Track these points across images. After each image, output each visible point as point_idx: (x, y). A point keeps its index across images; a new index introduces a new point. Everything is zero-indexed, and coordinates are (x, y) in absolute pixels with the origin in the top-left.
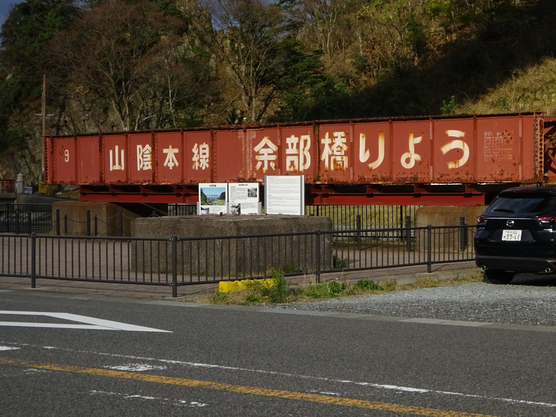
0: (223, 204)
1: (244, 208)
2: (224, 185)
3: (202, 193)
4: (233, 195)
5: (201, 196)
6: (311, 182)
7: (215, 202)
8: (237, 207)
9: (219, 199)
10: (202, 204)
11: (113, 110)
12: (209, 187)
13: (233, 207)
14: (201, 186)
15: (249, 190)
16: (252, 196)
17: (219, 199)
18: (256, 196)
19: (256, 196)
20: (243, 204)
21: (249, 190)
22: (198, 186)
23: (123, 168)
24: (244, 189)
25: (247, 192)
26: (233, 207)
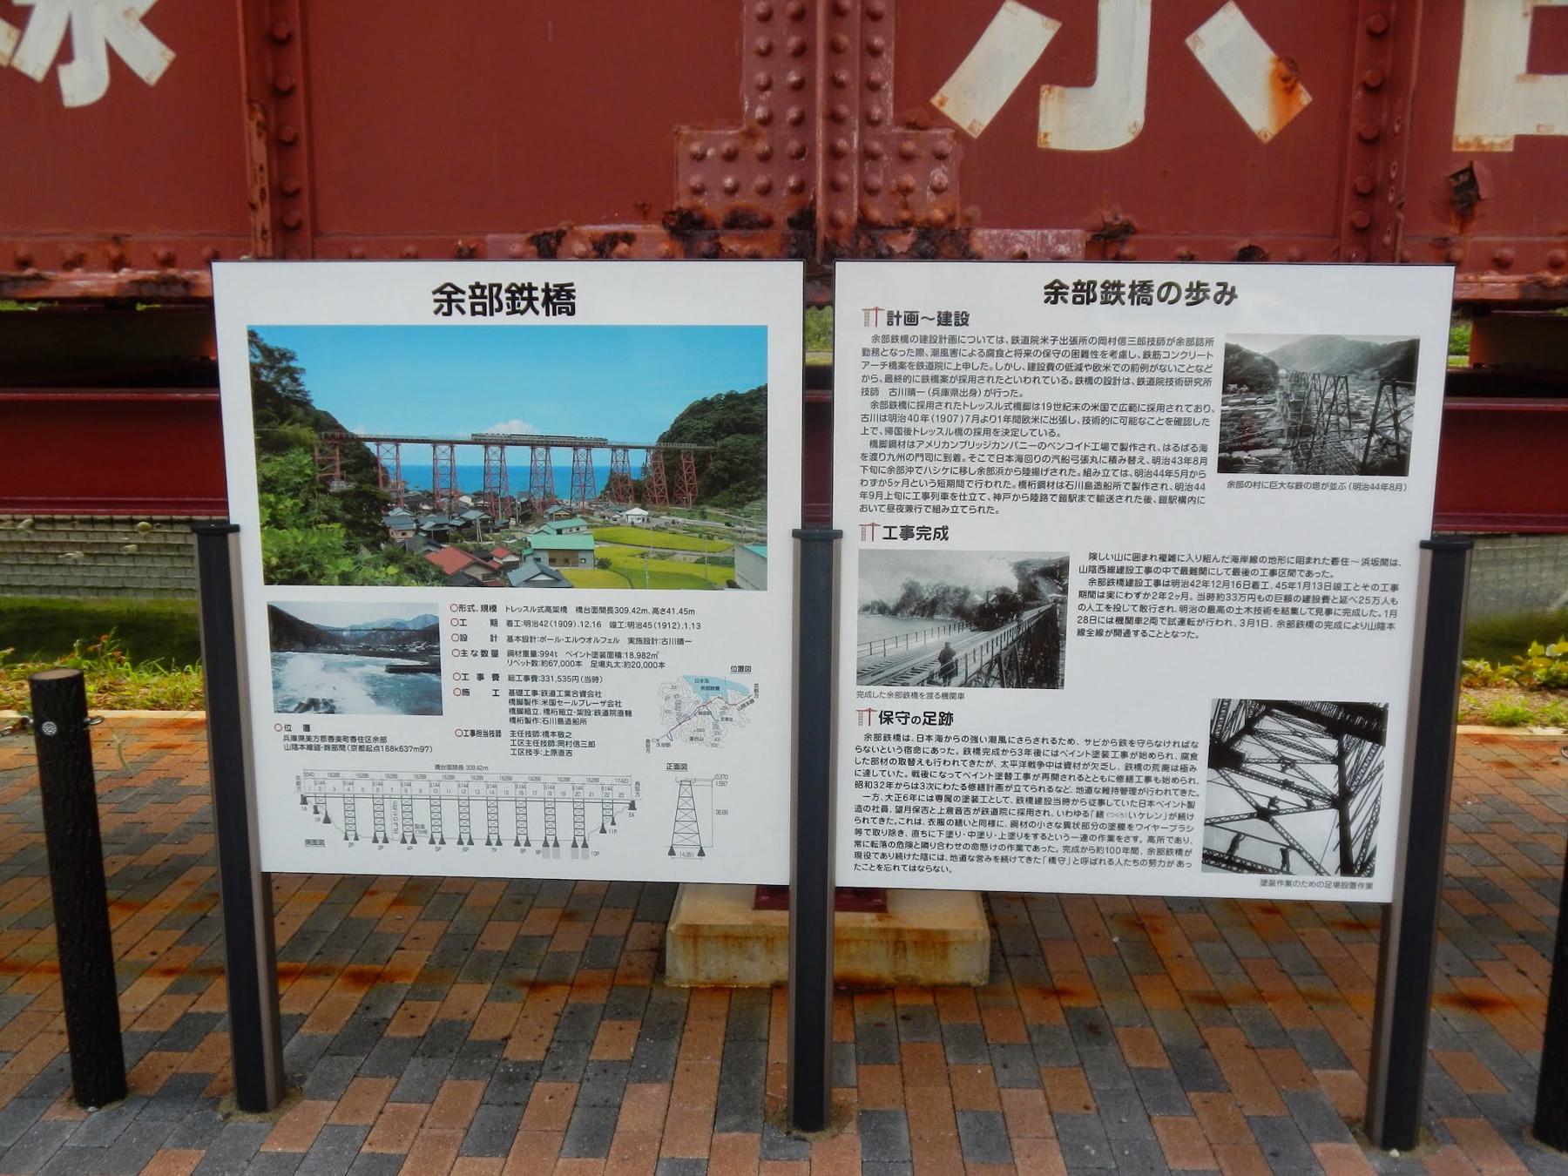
0: (722, 572)
1: (1123, 626)
2: (764, 291)
3: (278, 403)
4: (929, 433)
5: (267, 445)
6: (685, 912)
7: (543, 538)
8: (987, 616)
9: (624, 489)
10: (281, 571)
11: (196, 277)
12: (423, 312)
13: (918, 606)
14: (254, 298)
15: (1244, 374)
16: (1309, 463)
17: (624, 489)
18: (1396, 464)
19: (1396, 464)
20: (1113, 574)
21: (1244, 374)
22: (201, 311)
23: (1380, 886)
24: (1149, 362)
25: (1212, 395)
26: (918, 606)
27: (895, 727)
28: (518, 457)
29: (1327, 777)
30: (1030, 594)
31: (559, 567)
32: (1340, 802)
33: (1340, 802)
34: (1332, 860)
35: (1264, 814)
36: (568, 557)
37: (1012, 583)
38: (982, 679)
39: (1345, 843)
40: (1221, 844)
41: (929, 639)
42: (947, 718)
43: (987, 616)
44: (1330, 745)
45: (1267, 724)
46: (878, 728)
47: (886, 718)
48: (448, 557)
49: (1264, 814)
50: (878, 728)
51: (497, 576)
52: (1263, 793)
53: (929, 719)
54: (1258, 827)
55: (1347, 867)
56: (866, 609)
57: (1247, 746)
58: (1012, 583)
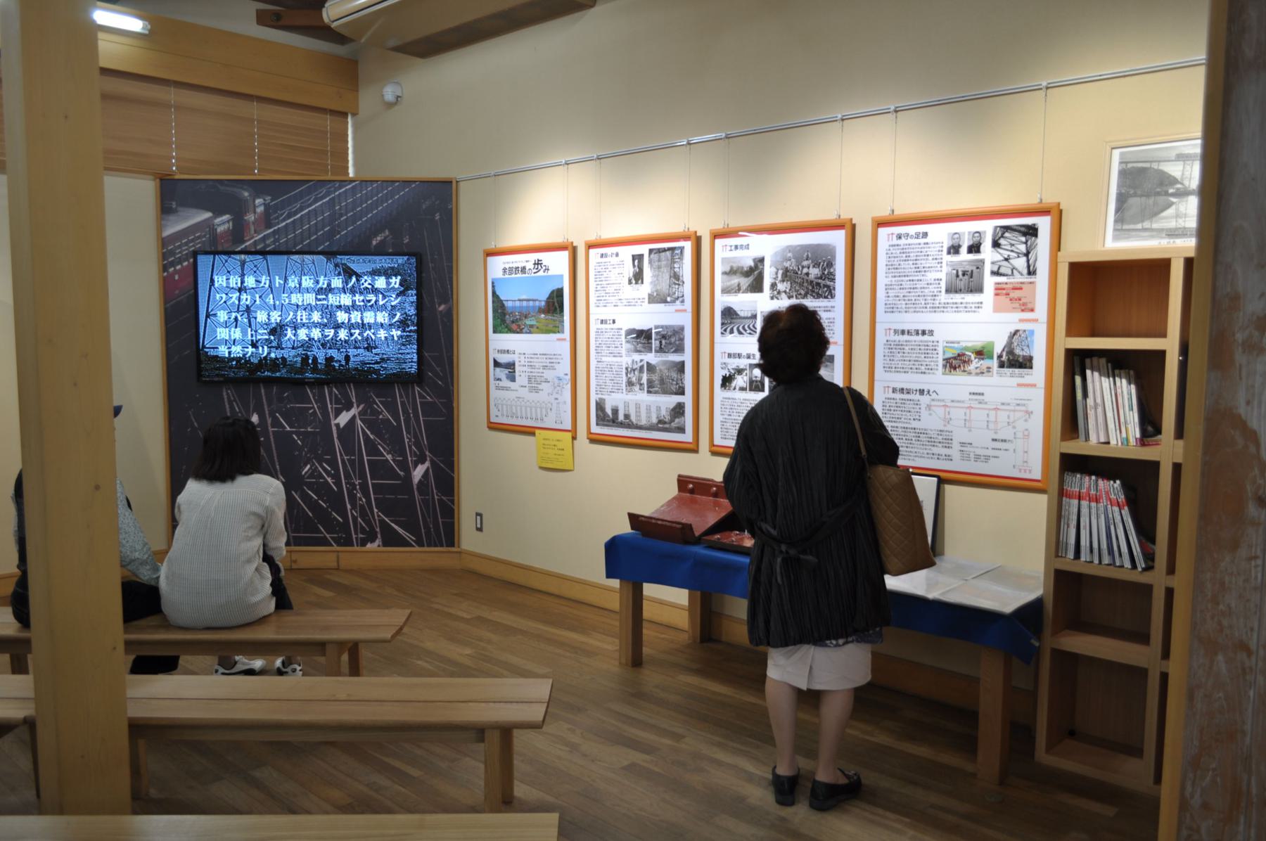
7: (528, 322)
9: (541, 311)
27: (903, 241)
28: (525, 304)
29: (1023, 248)
30: (756, 267)
31: (531, 330)
32: (1027, 255)
33: (1027, 255)
34: (1025, 271)
35: (1006, 260)
36: (531, 326)
37: (752, 264)
38: (746, 291)
39: (1029, 267)
40: (995, 269)
41: (736, 280)
42: (925, 235)
43: (748, 273)
44: (1023, 239)
45: (1007, 235)
46: (895, 241)
47: (899, 237)
48: (514, 326)
49: (1006, 260)
50: (895, 241)
51: (521, 332)
52: (1006, 254)
53: (917, 236)
54: (1005, 263)
55: (1029, 273)
56: (725, 273)
57: (1002, 241)
58: (752, 264)
